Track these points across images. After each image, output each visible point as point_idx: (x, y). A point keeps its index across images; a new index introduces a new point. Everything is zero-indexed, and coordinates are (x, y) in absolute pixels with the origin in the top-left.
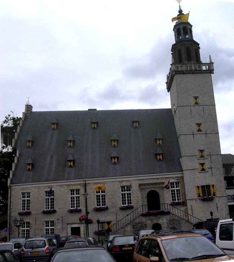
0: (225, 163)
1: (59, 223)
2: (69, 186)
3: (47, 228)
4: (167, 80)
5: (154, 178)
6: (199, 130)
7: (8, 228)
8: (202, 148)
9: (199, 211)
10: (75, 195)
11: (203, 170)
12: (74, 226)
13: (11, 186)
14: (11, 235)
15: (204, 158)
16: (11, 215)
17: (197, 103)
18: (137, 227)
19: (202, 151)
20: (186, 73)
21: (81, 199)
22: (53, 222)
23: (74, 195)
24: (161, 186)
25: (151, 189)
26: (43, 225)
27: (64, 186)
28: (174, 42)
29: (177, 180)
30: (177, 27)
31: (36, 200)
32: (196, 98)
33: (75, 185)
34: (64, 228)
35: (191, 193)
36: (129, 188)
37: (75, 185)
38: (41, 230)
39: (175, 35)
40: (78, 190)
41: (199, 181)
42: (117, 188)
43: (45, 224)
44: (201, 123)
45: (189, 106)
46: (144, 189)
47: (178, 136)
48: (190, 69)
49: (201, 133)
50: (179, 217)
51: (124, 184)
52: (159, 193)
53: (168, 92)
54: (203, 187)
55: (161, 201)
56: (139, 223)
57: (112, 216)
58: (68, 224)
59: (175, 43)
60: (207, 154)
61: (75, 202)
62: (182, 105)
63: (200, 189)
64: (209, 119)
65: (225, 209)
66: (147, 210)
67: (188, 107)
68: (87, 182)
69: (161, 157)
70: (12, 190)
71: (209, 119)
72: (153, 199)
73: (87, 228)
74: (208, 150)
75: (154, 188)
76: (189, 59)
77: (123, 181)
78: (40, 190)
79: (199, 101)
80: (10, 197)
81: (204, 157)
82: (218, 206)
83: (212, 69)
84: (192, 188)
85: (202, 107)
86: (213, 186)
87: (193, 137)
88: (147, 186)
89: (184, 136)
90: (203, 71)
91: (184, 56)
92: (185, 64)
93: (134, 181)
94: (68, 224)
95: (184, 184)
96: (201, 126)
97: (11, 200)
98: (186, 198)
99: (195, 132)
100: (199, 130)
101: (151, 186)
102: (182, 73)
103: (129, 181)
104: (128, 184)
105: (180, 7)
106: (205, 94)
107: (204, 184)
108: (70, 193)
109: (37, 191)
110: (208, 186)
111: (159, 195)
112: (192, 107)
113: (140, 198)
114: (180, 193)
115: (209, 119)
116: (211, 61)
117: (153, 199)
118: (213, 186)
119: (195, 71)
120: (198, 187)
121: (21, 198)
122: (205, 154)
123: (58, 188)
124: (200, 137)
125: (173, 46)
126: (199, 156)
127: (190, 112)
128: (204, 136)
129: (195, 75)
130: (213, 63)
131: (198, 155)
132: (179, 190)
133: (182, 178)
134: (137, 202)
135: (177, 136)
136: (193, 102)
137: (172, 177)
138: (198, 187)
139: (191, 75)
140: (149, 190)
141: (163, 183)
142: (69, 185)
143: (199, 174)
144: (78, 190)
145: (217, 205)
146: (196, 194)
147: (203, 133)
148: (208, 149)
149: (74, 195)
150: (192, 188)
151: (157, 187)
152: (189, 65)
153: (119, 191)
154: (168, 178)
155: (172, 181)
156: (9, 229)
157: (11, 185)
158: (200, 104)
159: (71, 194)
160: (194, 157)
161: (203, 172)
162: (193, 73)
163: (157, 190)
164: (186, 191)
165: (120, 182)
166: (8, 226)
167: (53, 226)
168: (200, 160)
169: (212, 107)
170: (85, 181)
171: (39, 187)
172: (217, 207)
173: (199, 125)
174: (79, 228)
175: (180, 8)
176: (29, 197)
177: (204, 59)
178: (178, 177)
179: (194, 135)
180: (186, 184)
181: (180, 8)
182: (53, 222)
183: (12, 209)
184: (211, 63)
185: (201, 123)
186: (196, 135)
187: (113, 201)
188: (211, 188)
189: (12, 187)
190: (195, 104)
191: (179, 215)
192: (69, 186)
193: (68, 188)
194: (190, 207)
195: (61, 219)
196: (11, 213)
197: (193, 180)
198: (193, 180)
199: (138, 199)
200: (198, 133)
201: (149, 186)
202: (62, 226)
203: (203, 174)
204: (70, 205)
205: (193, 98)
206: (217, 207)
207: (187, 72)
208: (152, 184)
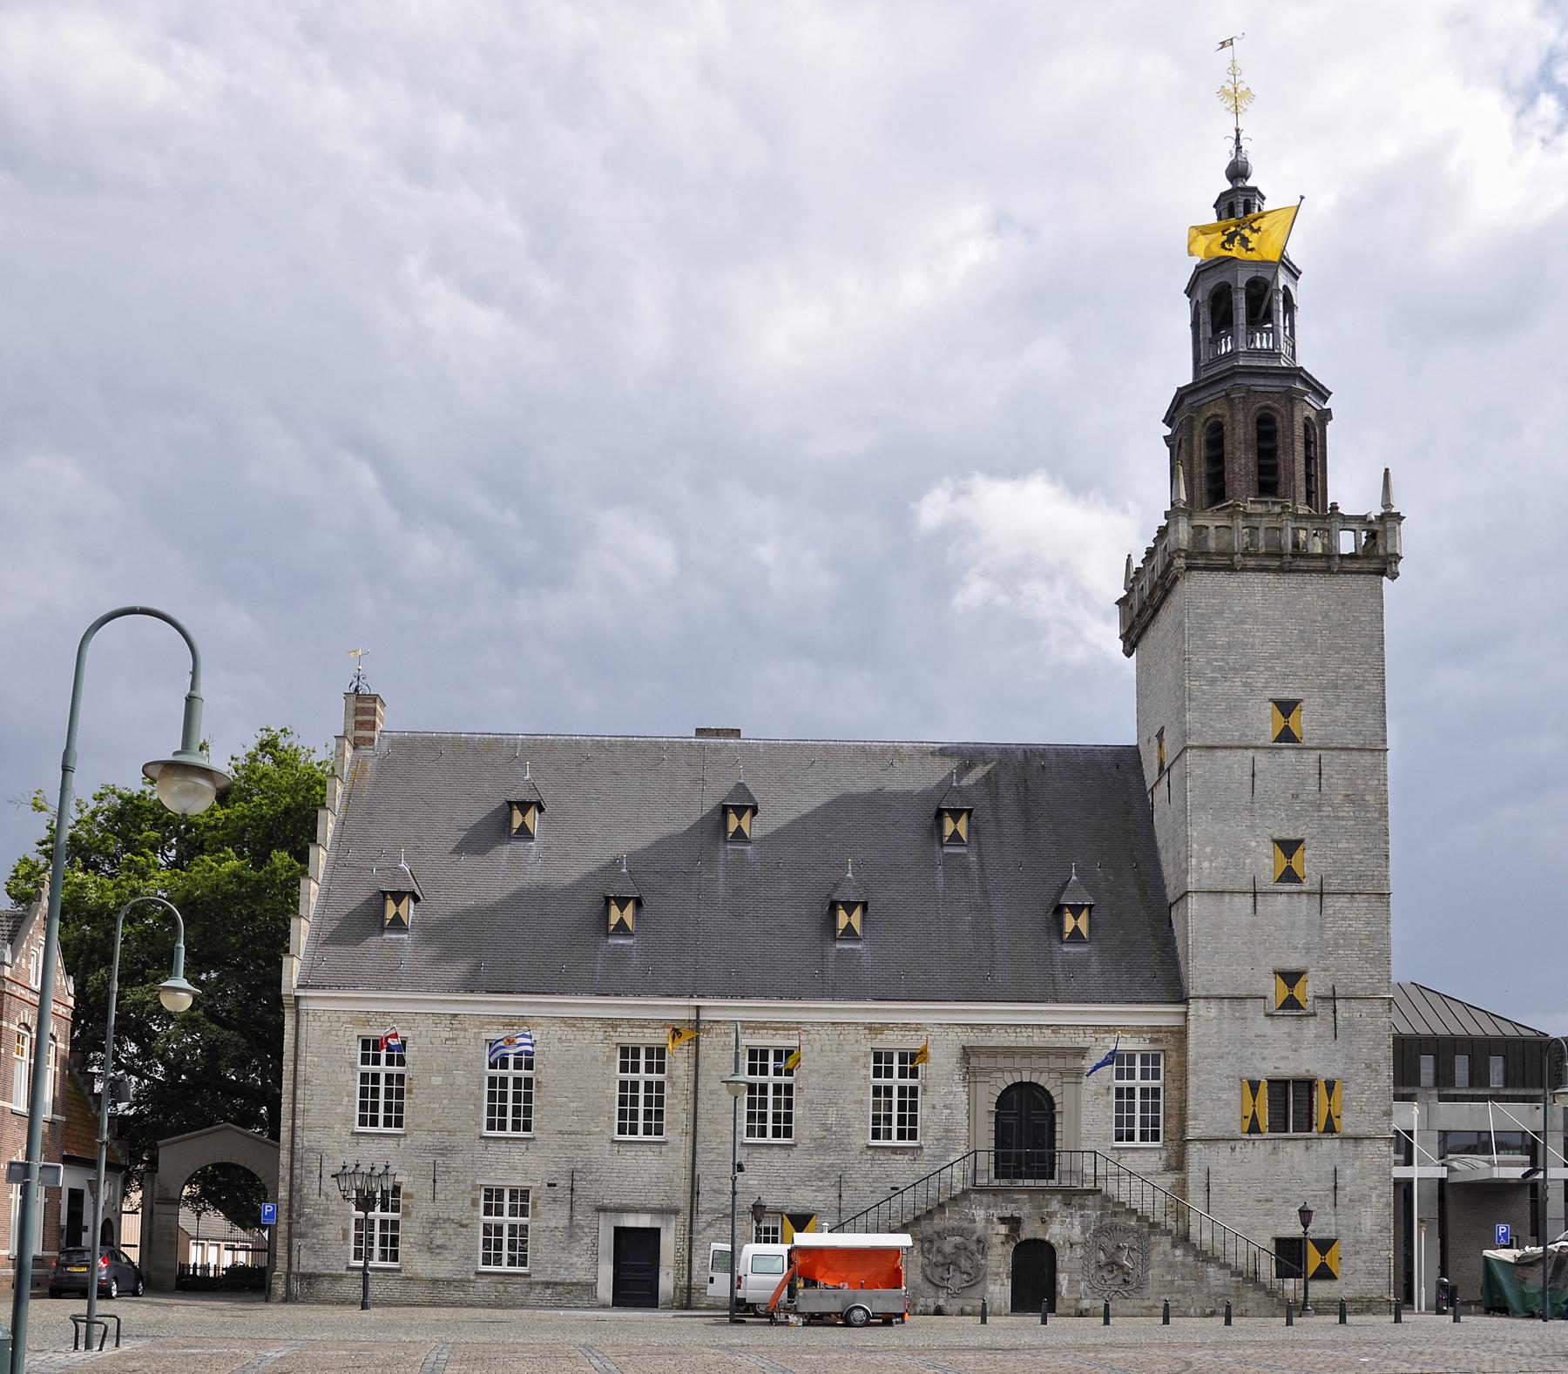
0: (1405, 1030)
1: (555, 1200)
2: (614, 1027)
3: (493, 1219)
4: (1130, 591)
6: (1289, 876)
7: (284, 1207)
8: (1293, 964)
9: (1249, 1191)
12: (630, 1221)
13: (297, 998)
14: (295, 1241)
16: (297, 1140)
17: (1287, 736)
18: (939, 1251)
19: (1291, 977)
21: (674, 1096)
22: (525, 1194)
23: (501, 1214)
24: (1072, 1063)
28: (1187, 378)
29: (1152, 1041)
30: (1211, 283)
31: (436, 1080)
32: (1286, 707)
33: (644, 1027)
34: (582, 1227)
35: (1215, 1103)
36: (911, 1061)
37: (644, 1024)
38: (463, 1226)
39: (1195, 325)
42: (855, 1060)
43: (482, 1202)
44: (1299, 837)
45: (1247, 748)
46: (987, 1072)
47: (1171, 900)
48: (1267, 545)
49: (1294, 887)
50: (1143, 1219)
51: (892, 1041)
52: (1056, 1100)
53: (1129, 655)
54: (1279, 1087)
55: (1063, 1139)
56: (954, 1231)
57: (820, 1189)
58: (602, 1209)
59: (1191, 381)
61: (641, 1108)
62: (1209, 743)
63: (1263, 1091)
65: (1374, 1199)
67: (1239, 752)
68: (705, 1016)
69: (1083, 923)
70: (303, 1018)
71: (1343, 818)
72: (1025, 1130)
75: (1033, 1070)
76: (1268, 485)
77: (885, 1026)
78: (462, 1034)
79: (1302, 722)
80: (296, 1055)
83: (1389, 550)
84: (1222, 1089)
85: (1314, 755)
86: (1330, 1086)
87: (1250, 910)
88: (1002, 1062)
90: (1337, 560)
91: (1241, 463)
92: (1247, 515)
93: (938, 1027)
94: (602, 1209)
95: (1183, 1065)
97: (301, 1067)
98: (1184, 1132)
99: (1267, 879)
100: (1289, 876)
101: (1018, 1062)
102: (1225, 563)
103: (918, 1028)
104: (912, 1043)
105: (1238, 139)
106: (1336, 687)
108: (618, 1060)
109: (447, 1035)
111: (1053, 1105)
112: (1262, 759)
113: (961, 1116)
114: (1156, 1108)
116: (1387, 503)
117: (1025, 1130)
118: (1330, 1086)
119: (1294, 556)
120: (1254, 1086)
121: (353, 1065)
122: (1307, 990)
123: (558, 1031)
125: (1182, 395)
126: (1274, 1001)
127: (1248, 778)
129: (1292, 580)
130: (1398, 518)
131: (1271, 995)
132: (1156, 1091)
133: (1181, 1033)
134: (947, 1131)
135: (1164, 897)
136: (1268, 724)
137: (1128, 1023)
138: (1254, 1086)
139: (1270, 577)
140: (1010, 1080)
141: (1082, 1052)
142: (613, 1024)
143: (1268, 1022)
146: (1238, 1116)
147: (1305, 887)
148: (1327, 970)
149: (501, 1214)
150: (1222, 1089)
151: (1050, 1071)
152: (1265, 522)
153: (863, 1072)
154: (1109, 1029)
155: (1128, 1044)
156: (290, 1210)
157: (301, 993)
159: (624, 1069)
164: (1191, 1097)
165: (873, 1029)
166: (283, 1193)
167: (524, 1214)
168: (1278, 1021)
169: (1367, 759)
173: (1289, 847)
175: (1239, 148)
177: (1350, 487)
178: (1158, 1029)
180: (1195, 1073)
181: (1239, 148)
182: (525, 1194)
184: (1391, 518)
185: (1302, 841)
186: (1269, 898)
187: (832, 1120)
188: (1264, 1121)
189: (303, 1005)
191: (1148, 1207)
192: (614, 1027)
194: (1203, 1175)
195: (563, 1182)
196: (299, 1132)
197: (1232, 1051)
198: (1232, 1051)
199: (956, 1116)
200: (1287, 887)
201: (1008, 1063)
202: (571, 1217)
203: (1285, 1026)
208: (1028, 1052)
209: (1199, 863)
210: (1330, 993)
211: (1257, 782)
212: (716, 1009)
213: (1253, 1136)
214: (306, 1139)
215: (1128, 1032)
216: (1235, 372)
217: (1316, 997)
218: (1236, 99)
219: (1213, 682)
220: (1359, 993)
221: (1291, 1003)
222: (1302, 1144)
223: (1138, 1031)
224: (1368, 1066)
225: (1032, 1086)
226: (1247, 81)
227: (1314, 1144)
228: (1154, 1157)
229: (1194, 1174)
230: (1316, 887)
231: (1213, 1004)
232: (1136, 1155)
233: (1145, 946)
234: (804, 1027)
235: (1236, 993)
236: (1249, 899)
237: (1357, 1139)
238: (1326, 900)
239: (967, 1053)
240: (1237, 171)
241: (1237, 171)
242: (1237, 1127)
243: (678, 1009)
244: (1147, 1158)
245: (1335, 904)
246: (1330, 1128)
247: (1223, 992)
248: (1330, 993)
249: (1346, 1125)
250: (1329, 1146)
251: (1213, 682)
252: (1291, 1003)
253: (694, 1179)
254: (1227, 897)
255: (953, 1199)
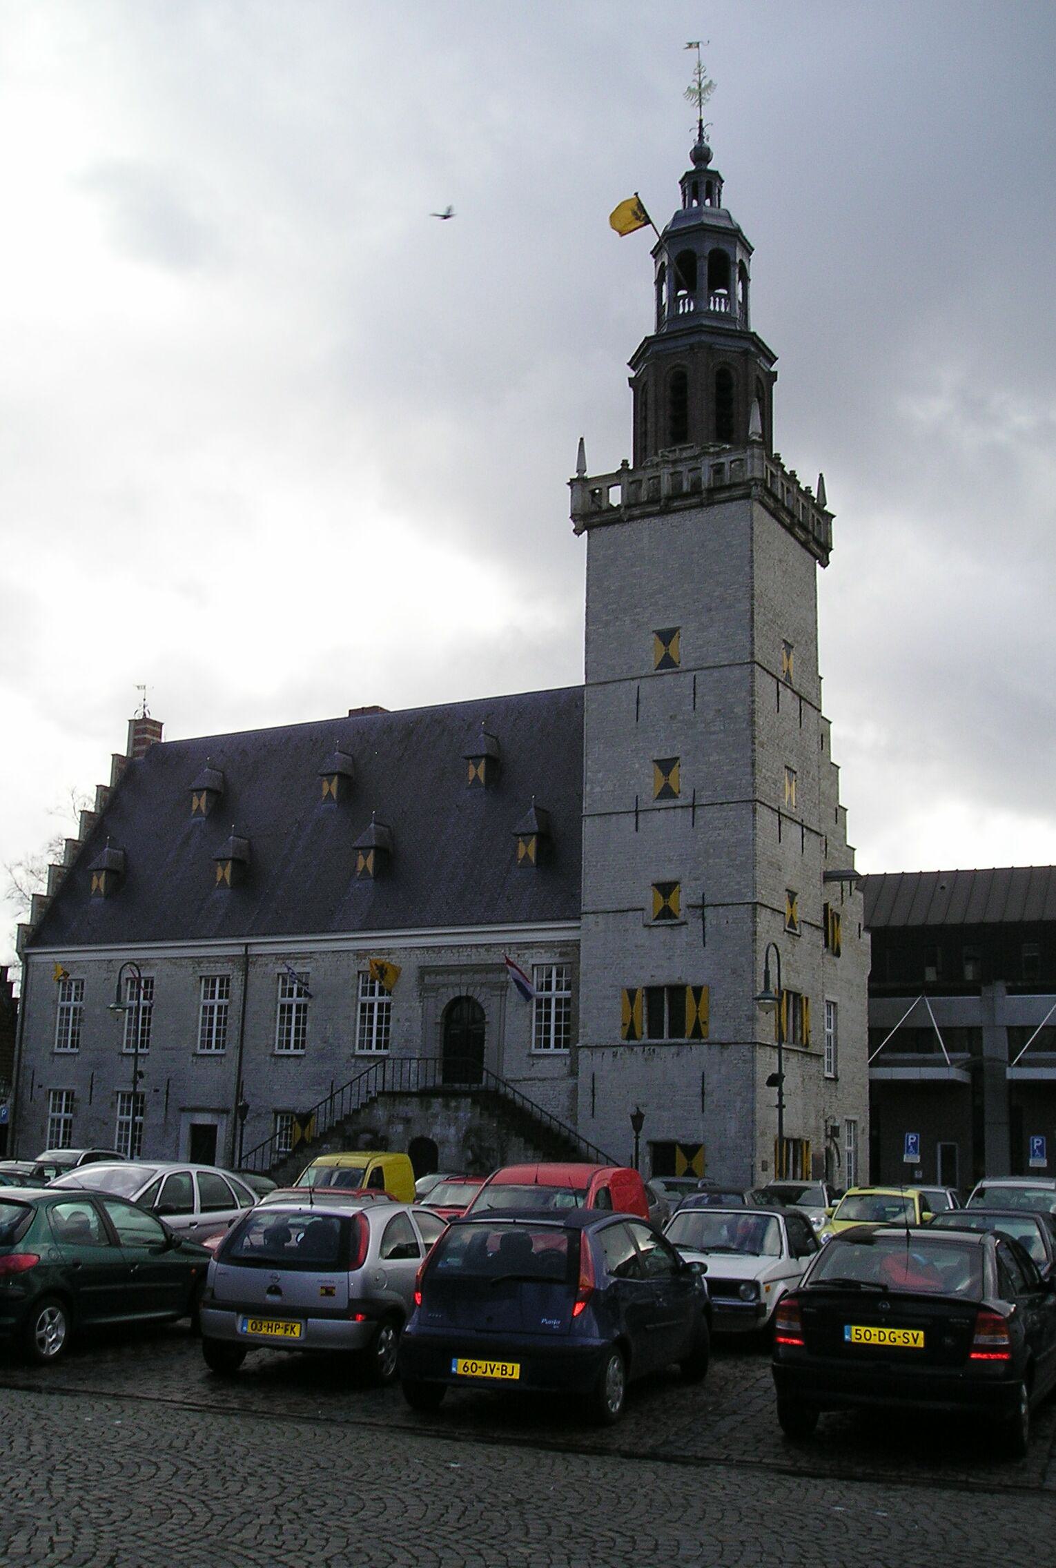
5: (477, 946)
8: (668, 877)
10: (217, 1001)
11: (666, 913)
15: (676, 921)
17: (667, 662)
19: (666, 889)
20: (632, 519)
25: (457, 989)
26: (113, 1105)
27: (184, 962)
29: (562, 954)
35: (601, 1015)
40: (225, 981)
41: (642, 968)
45: (633, 679)
49: (671, 803)
54: (653, 993)
58: (183, 1110)
60: (691, 902)
62: (602, 679)
64: (713, 737)
65: (738, 1104)
66: (439, 1080)
67: (627, 684)
71: (714, 733)
73: (239, 1133)
74: (693, 884)
79: (680, 649)
81: (674, 796)
82: (708, 1088)
85: (690, 676)
86: (698, 991)
89: (597, 820)
91: (701, 406)
94: (183, 1110)
96: (675, 769)
99: (648, 800)
100: (667, 792)
107: (663, 978)
109: (105, 976)
110: (677, 991)
112: (646, 686)
113: (417, 1028)
115: (714, 733)
118: (698, 991)
120: (632, 994)
122: (682, 900)
124: (666, 824)
128: (683, 817)
129: (674, 519)
131: (649, 906)
136: (652, 651)
139: (654, 521)
143: (646, 931)
144: (225, 981)
145: (706, 1081)
147: (679, 803)
148: (696, 879)
158: (682, 666)
160: (630, 913)
161: (663, 922)
162: (666, 511)
163: (480, 996)
168: (654, 930)
170: (247, 945)
171: (110, 961)
172: (703, 1093)
173: (666, 765)
174: (212, 1129)
176: (79, 997)
179: (641, 816)
183: (28, 1038)
186: (649, 815)
188: (643, 1026)
190: (660, 667)
193: (195, 972)
195: (163, 1089)
203: (662, 934)
204: (196, 1036)
205: (654, 636)
206: (703, 1093)
207: (636, 512)
209: (592, 789)
210: (700, 902)
211: (642, 708)
212: (265, 946)
213: (632, 1042)
214: (28, 1058)
215: (542, 947)
216: (700, 329)
217: (689, 907)
218: (699, 93)
219: (607, 624)
220: (727, 900)
221: (666, 913)
222: (674, 1049)
223: (548, 946)
224: (734, 972)
225: (468, 998)
226: (710, 75)
227: (685, 1050)
228: (559, 1063)
229: (584, 1079)
230: (690, 800)
231: (600, 918)
232: (547, 1061)
233: (555, 867)
234: (316, 956)
235: (621, 907)
236: (631, 819)
237: (723, 1045)
238: (698, 811)
239: (424, 971)
240: (701, 155)
241: (701, 155)
242: (618, 1034)
243: (230, 948)
244: (554, 1060)
245: (706, 814)
246: (697, 1033)
247: (609, 907)
248: (700, 902)
249: (714, 1029)
250: (699, 1054)
251: (607, 624)
252: (666, 913)
253: (240, 1085)
254: (614, 818)
255: (364, 1105)
